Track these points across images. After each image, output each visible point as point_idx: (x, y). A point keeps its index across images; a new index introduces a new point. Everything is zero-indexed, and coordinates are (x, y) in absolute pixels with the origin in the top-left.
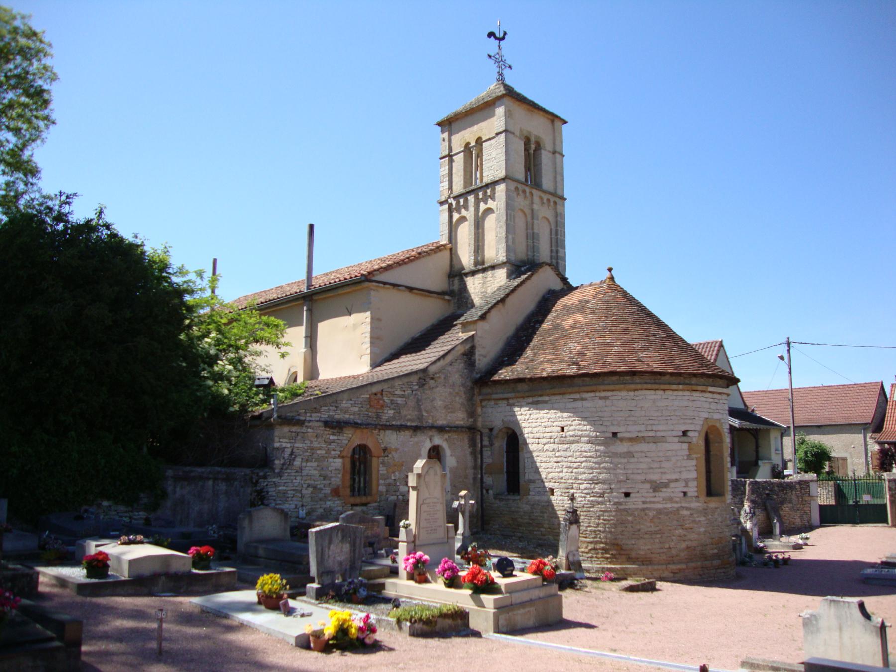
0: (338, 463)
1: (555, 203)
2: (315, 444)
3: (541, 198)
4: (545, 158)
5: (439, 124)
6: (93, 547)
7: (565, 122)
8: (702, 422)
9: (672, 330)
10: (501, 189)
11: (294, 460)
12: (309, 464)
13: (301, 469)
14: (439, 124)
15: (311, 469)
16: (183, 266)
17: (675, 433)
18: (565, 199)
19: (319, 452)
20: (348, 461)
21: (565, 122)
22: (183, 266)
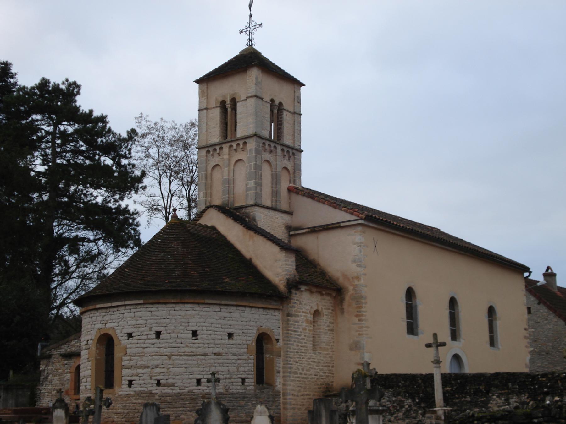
0: (69, 375)
1: (293, 154)
2: (58, 367)
3: (283, 150)
4: (287, 117)
5: (197, 82)
6: (46, 401)
7: (303, 85)
8: (81, 385)
9: (399, 217)
10: (252, 144)
11: (48, 376)
12: (55, 378)
13: (51, 381)
14: (197, 82)
15: (56, 380)
16: (106, 116)
17: (225, 333)
18: (302, 151)
19: (60, 371)
20: (73, 374)
21: (303, 85)
22: (106, 116)
